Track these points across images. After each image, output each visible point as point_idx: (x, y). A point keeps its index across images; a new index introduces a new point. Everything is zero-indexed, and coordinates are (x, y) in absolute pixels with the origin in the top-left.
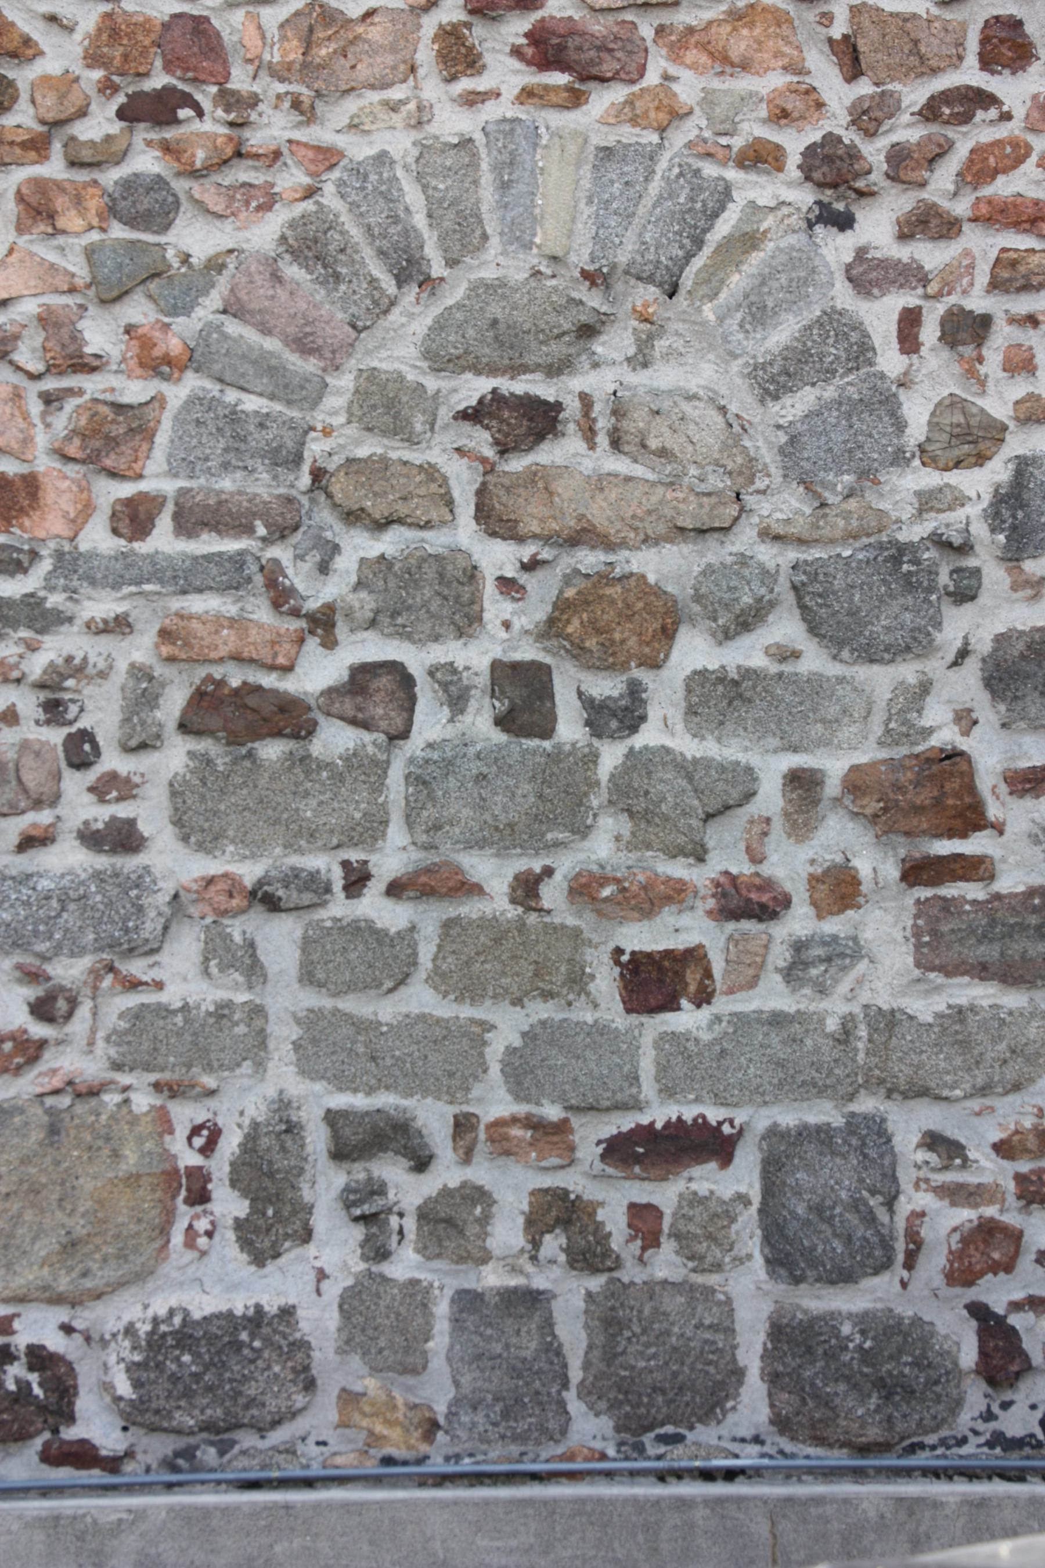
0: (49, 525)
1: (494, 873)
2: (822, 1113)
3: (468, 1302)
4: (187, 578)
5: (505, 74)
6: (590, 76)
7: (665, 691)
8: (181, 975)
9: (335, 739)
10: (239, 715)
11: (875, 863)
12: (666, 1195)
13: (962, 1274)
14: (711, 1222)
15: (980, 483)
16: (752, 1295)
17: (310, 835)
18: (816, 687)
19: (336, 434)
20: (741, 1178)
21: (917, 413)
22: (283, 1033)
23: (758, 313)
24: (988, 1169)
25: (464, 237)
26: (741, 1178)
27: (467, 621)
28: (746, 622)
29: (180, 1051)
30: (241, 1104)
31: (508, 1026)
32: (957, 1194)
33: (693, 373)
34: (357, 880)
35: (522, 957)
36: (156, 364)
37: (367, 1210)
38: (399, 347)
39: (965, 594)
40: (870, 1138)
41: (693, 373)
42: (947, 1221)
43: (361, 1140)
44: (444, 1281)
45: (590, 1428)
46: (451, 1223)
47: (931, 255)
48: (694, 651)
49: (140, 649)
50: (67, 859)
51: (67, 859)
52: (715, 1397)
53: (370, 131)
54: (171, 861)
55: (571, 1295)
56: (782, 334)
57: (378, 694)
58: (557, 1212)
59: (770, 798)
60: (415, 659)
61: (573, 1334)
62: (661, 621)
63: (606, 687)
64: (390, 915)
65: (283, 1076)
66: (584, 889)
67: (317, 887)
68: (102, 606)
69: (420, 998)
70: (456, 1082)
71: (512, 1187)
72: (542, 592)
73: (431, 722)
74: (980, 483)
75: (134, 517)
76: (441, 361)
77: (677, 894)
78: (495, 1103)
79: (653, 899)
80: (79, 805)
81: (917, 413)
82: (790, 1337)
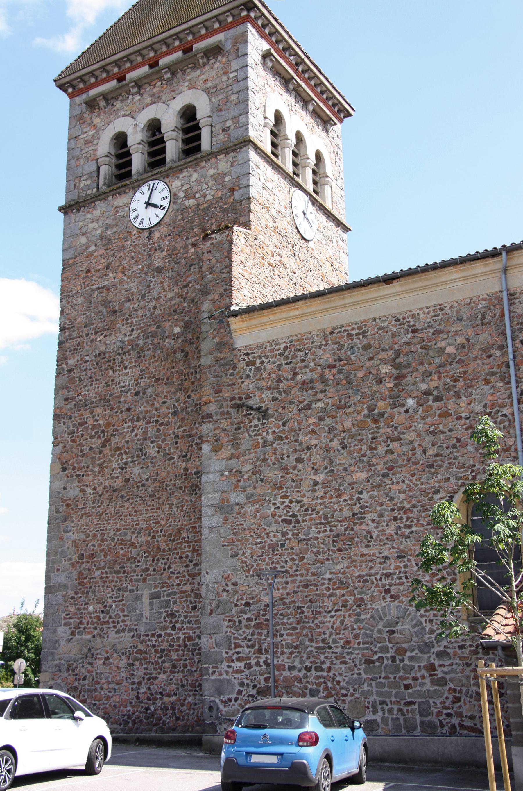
0: (352, 645)
1: (392, 676)
2: (423, 700)
3: (392, 719)
4: (364, 649)
5: (388, 599)
6: (395, 599)
7: (406, 658)
8: (366, 687)
9: (377, 664)
10: (369, 662)
11: (426, 675)
12: (409, 708)
13: (437, 716)
14: (413, 711)
15: (433, 636)
16: (418, 718)
17: (375, 673)
18: (420, 657)
19: (376, 635)
20: (416, 706)
21: (427, 629)
22: (375, 692)
23: (412, 620)
24: (439, 705)
25: (385, 615)
26: (416, 706)
27: (388, 652)
28: (413, 651)
29: (366, 694)
30: (371, 700)
31: (394, 691)
32: (436, 708)
33: (406, 626)
34: (380, 677)
35: (394, 685)
36: (360, 629)
37: (383, 710)
38: (380, 626)
39: (433, 647)
40: (428, 702)
41: (406, 626)
42: (435, 711)
43: (382, 703)
44: (390, 717)
45: (404, 731)
46: (390, 711)
47: (427, 614)
48: (408, 654)
49: (360, 656)
50: (355, 676)
51: (355, 676)
52: (415, 728)
53: (377, 606)
54: (364, 676)
55: (402, 718)
56: (414, 622)
57: (381, 659)
58: (400, 710)
59: (416, 668)
60: (384, 656)
61: (402, 722)
62: (405, 651)
63: (401, 658)
64: (382, 680)
65: (375, 697)
66: (400, 678)
67: (377, 678)
68: (357, 652)
69: (386, 689)
70: (390, 697)
71: (395, 707)
72: (395, 648)
73: (386, 662)
74: (433, 636)
75: (359, 643)
76: (384, 627)
77: (408, 678)
78: (393, 699)
79: (406, 679)
80: (356, 671)
81: (427, 629)
82: (422, 722)
